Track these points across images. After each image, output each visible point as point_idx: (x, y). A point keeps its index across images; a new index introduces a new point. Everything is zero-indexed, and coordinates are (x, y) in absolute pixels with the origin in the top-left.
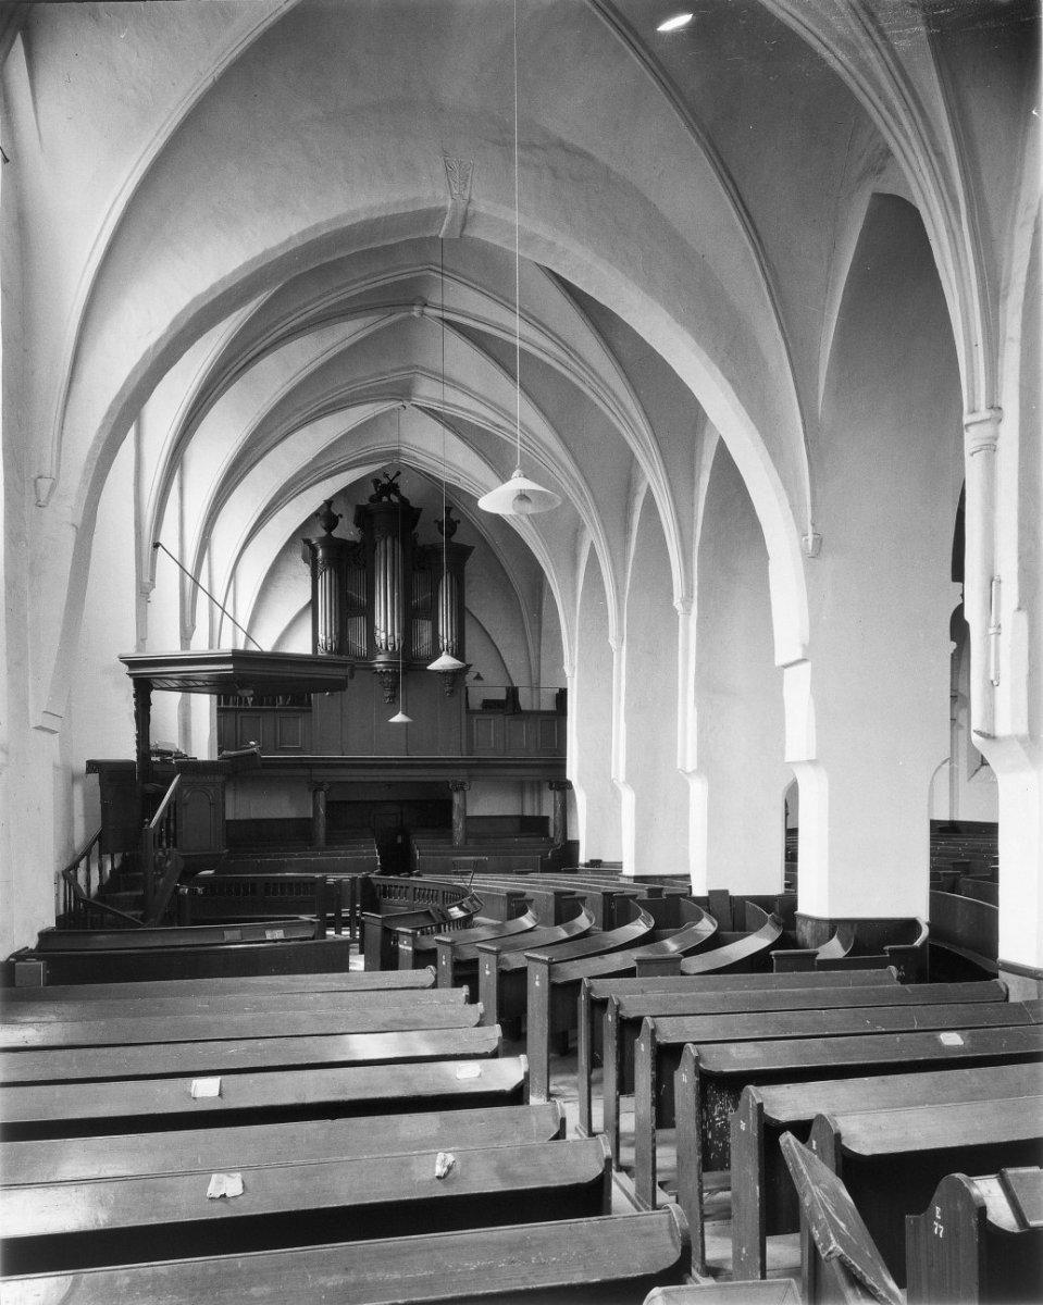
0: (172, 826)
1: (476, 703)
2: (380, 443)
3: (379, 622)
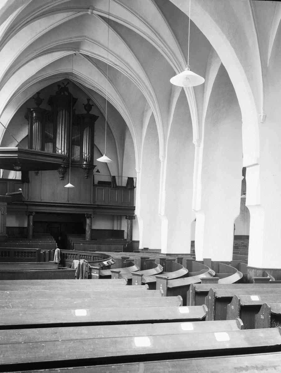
1: (96, 182)
2: (64, 69)
3: (58, 145)
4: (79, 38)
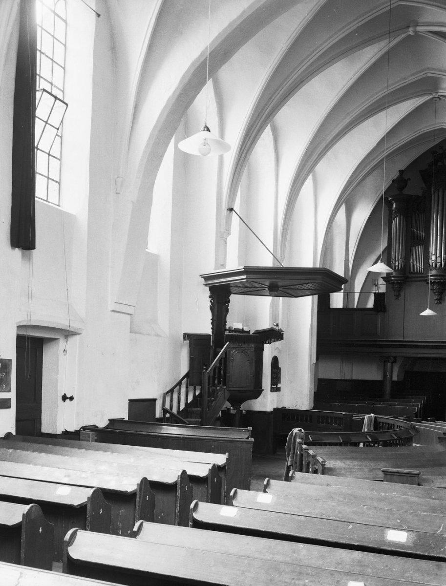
0: (222, 372)
3: (432, 249)
4: (419, 75)
